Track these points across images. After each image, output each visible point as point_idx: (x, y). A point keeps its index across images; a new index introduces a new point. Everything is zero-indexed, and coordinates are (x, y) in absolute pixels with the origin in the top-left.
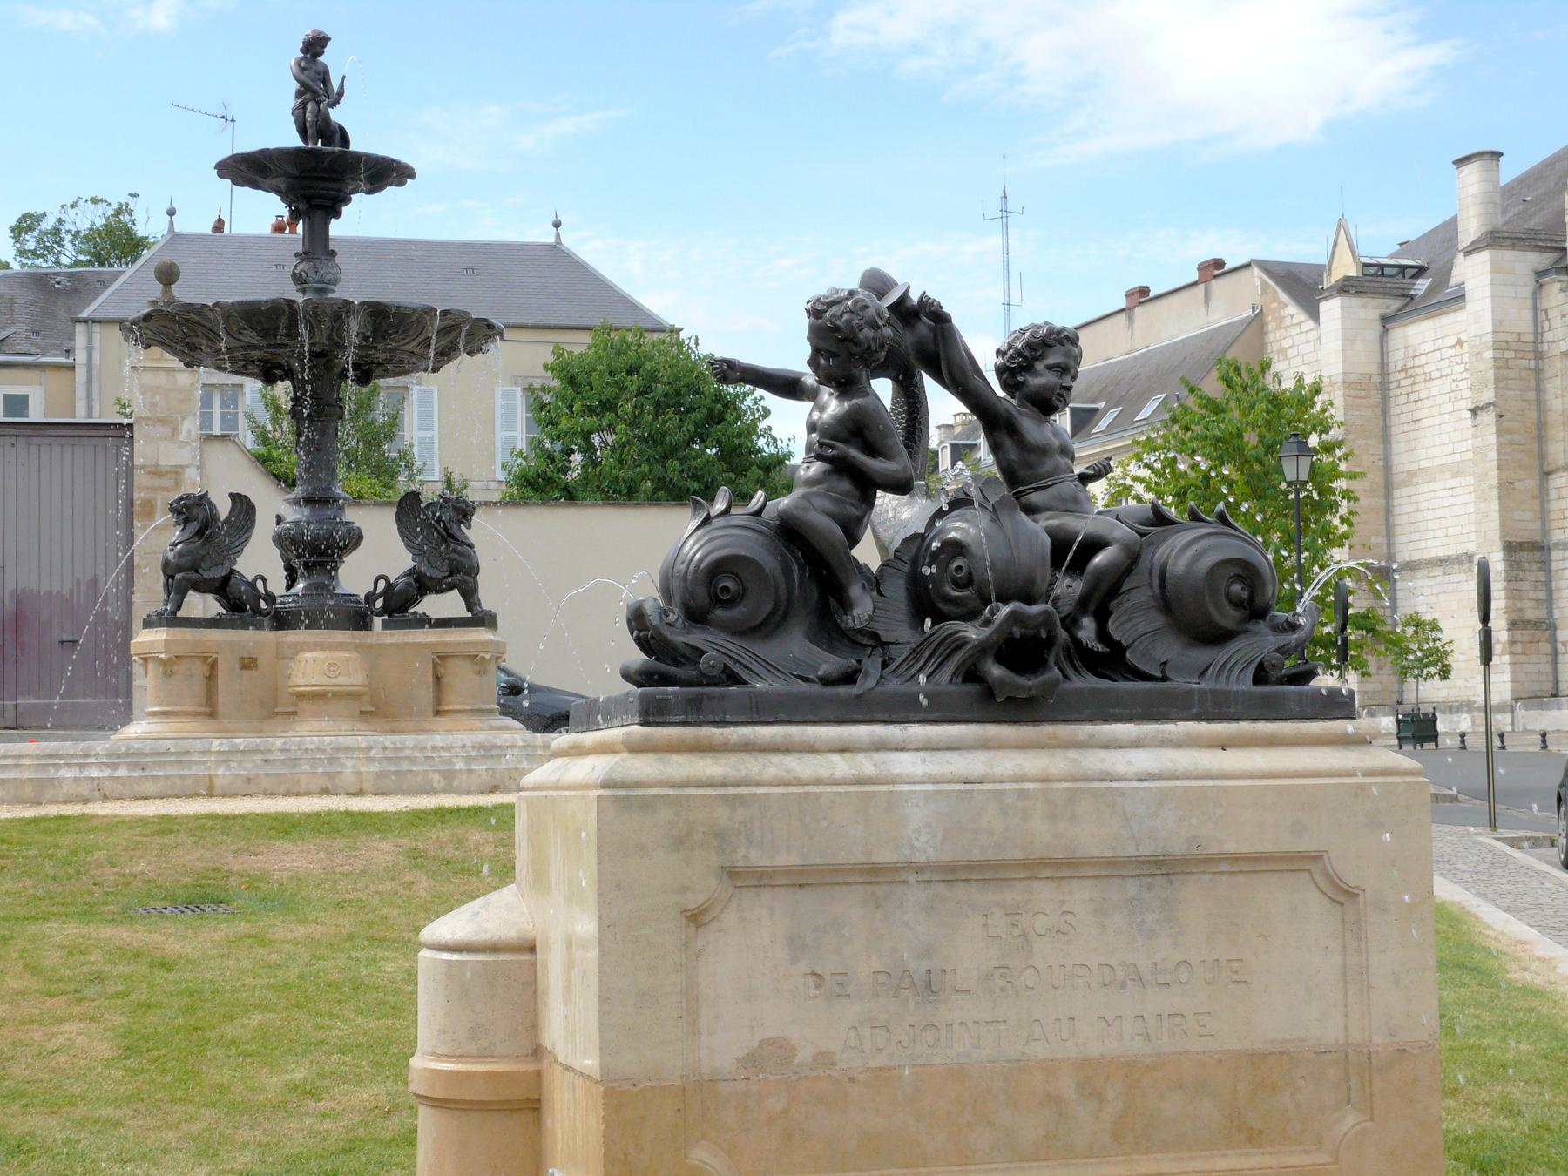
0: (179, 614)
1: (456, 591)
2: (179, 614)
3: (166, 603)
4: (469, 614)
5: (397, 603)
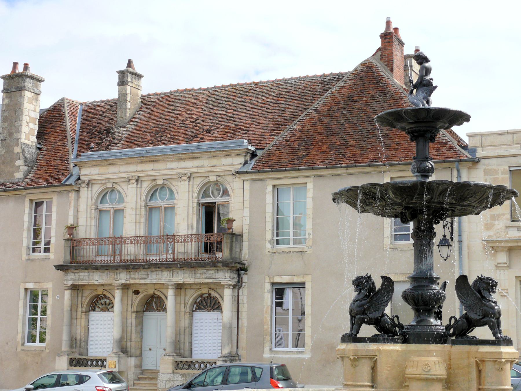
0: (359, 335)
1: (364, 325)
2: (359, 335)
3: (351, 330)
4: (494, 338)
5: (460, 332)
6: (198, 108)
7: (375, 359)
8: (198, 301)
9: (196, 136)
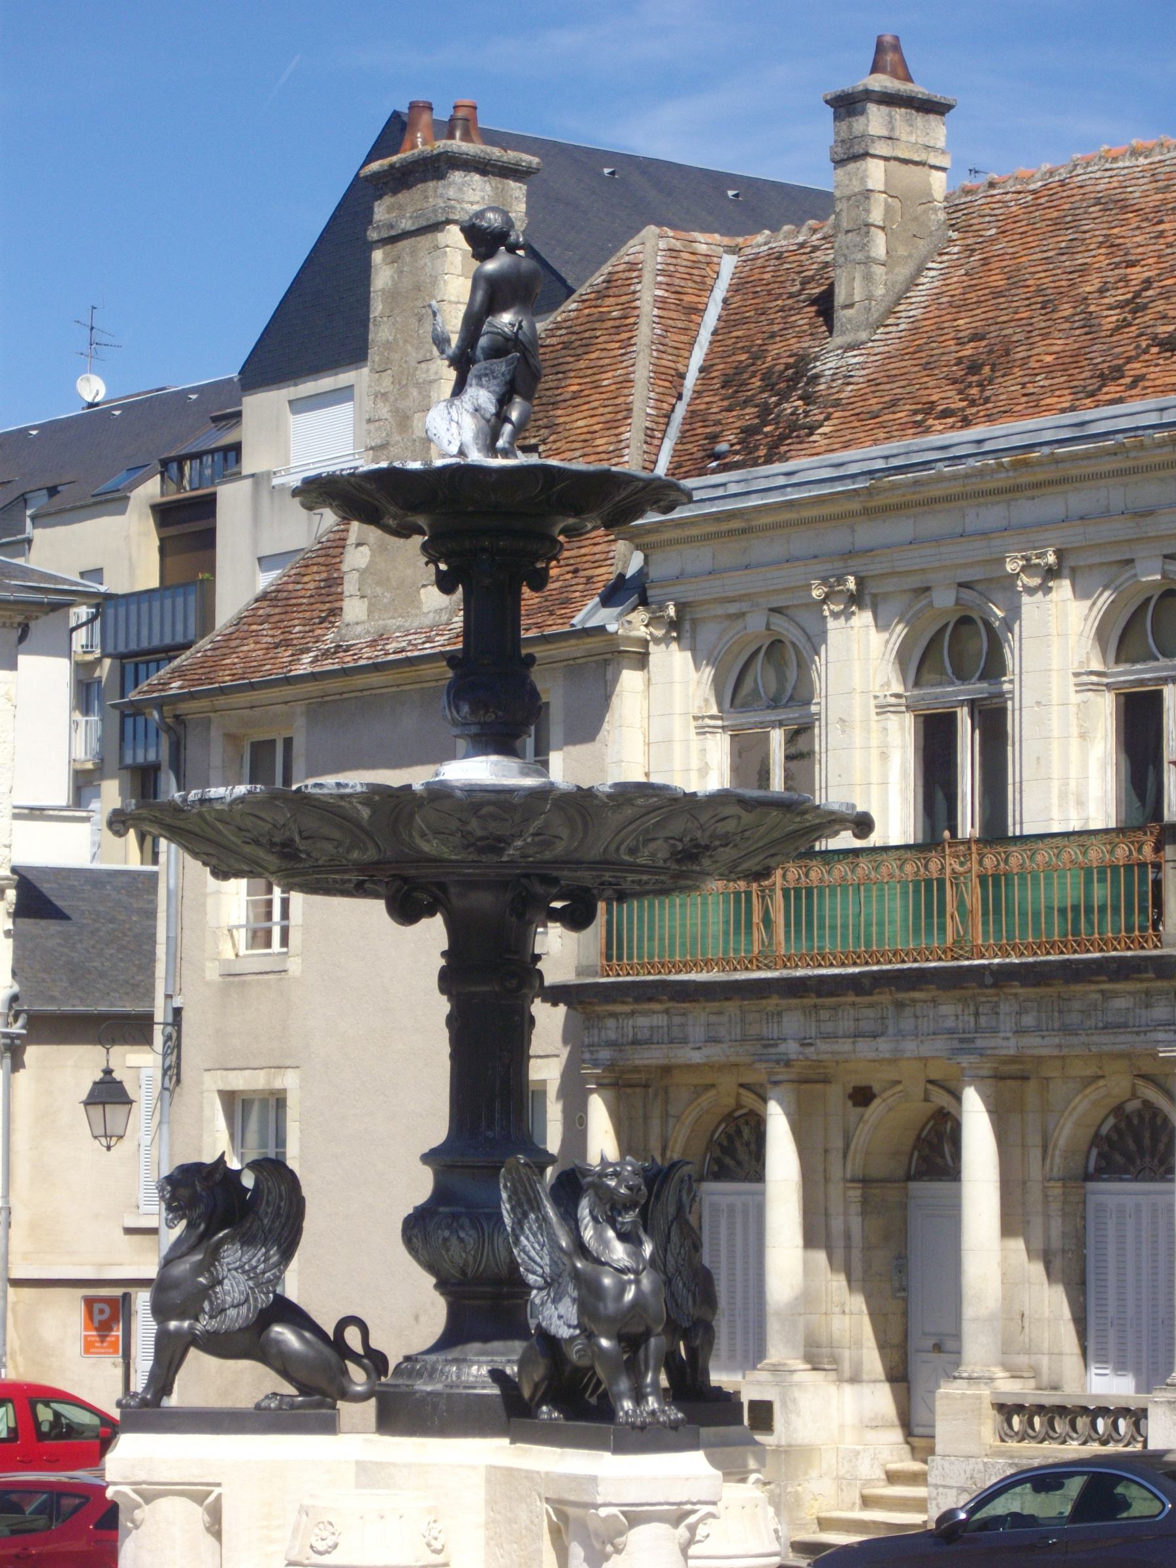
0: (173, 1401)
6: (1161, 235)
7: (211, 1498)
8: (1105, 1130)
9: (1117, 373)
